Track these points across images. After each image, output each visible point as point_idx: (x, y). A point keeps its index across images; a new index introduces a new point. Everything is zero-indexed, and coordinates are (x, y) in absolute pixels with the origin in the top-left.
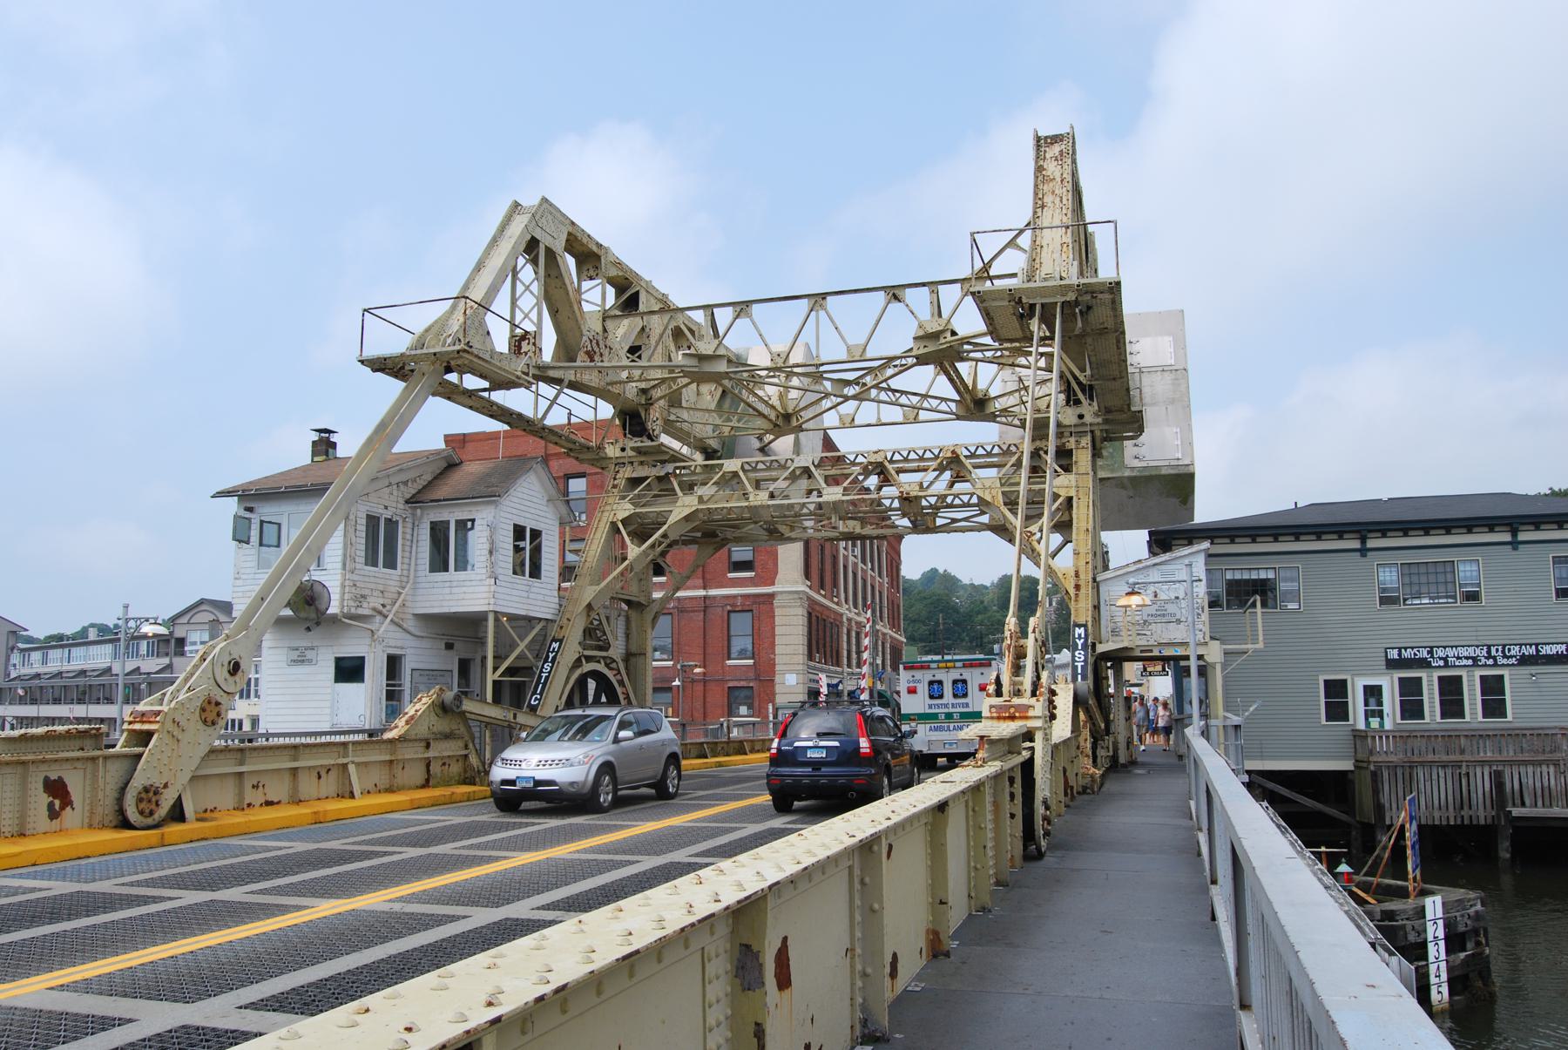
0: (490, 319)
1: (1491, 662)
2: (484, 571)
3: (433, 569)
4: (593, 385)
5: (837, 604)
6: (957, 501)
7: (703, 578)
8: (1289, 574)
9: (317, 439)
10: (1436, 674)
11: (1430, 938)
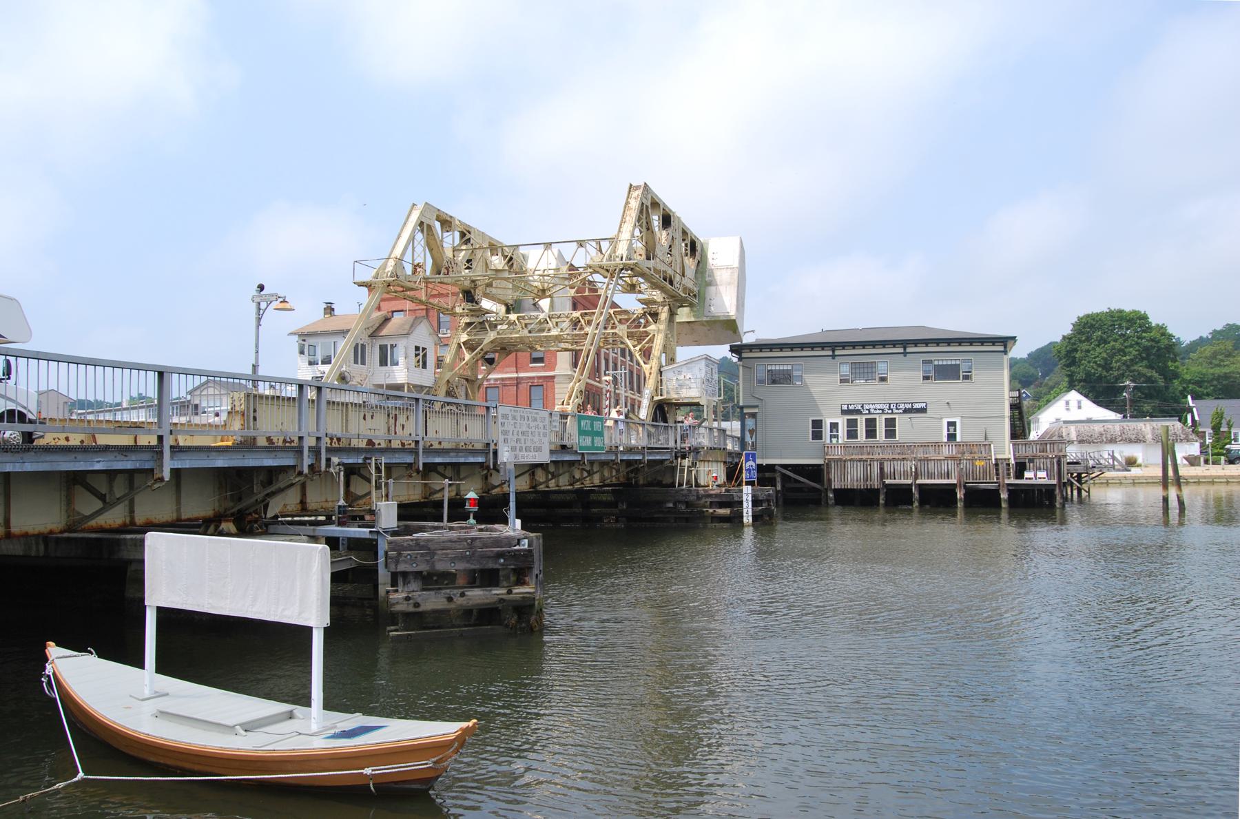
0: (405, 264)
1: (890, 411)
3: (381, 365)
7: (516, 367)
8: (798, 367)
10: (864, 417)
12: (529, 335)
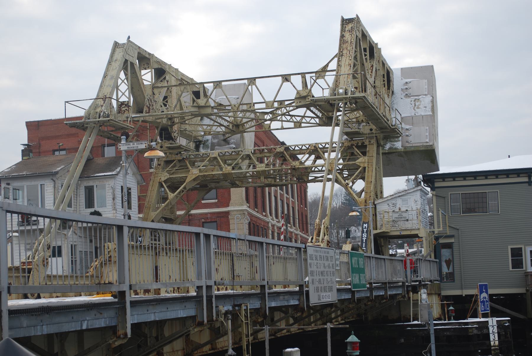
2: (111, 207)
4: (150, 120)
5: (265, 216)
6: (316, 169)
9: (23, 148)
11: (491, 332)
12: (233, 172)
